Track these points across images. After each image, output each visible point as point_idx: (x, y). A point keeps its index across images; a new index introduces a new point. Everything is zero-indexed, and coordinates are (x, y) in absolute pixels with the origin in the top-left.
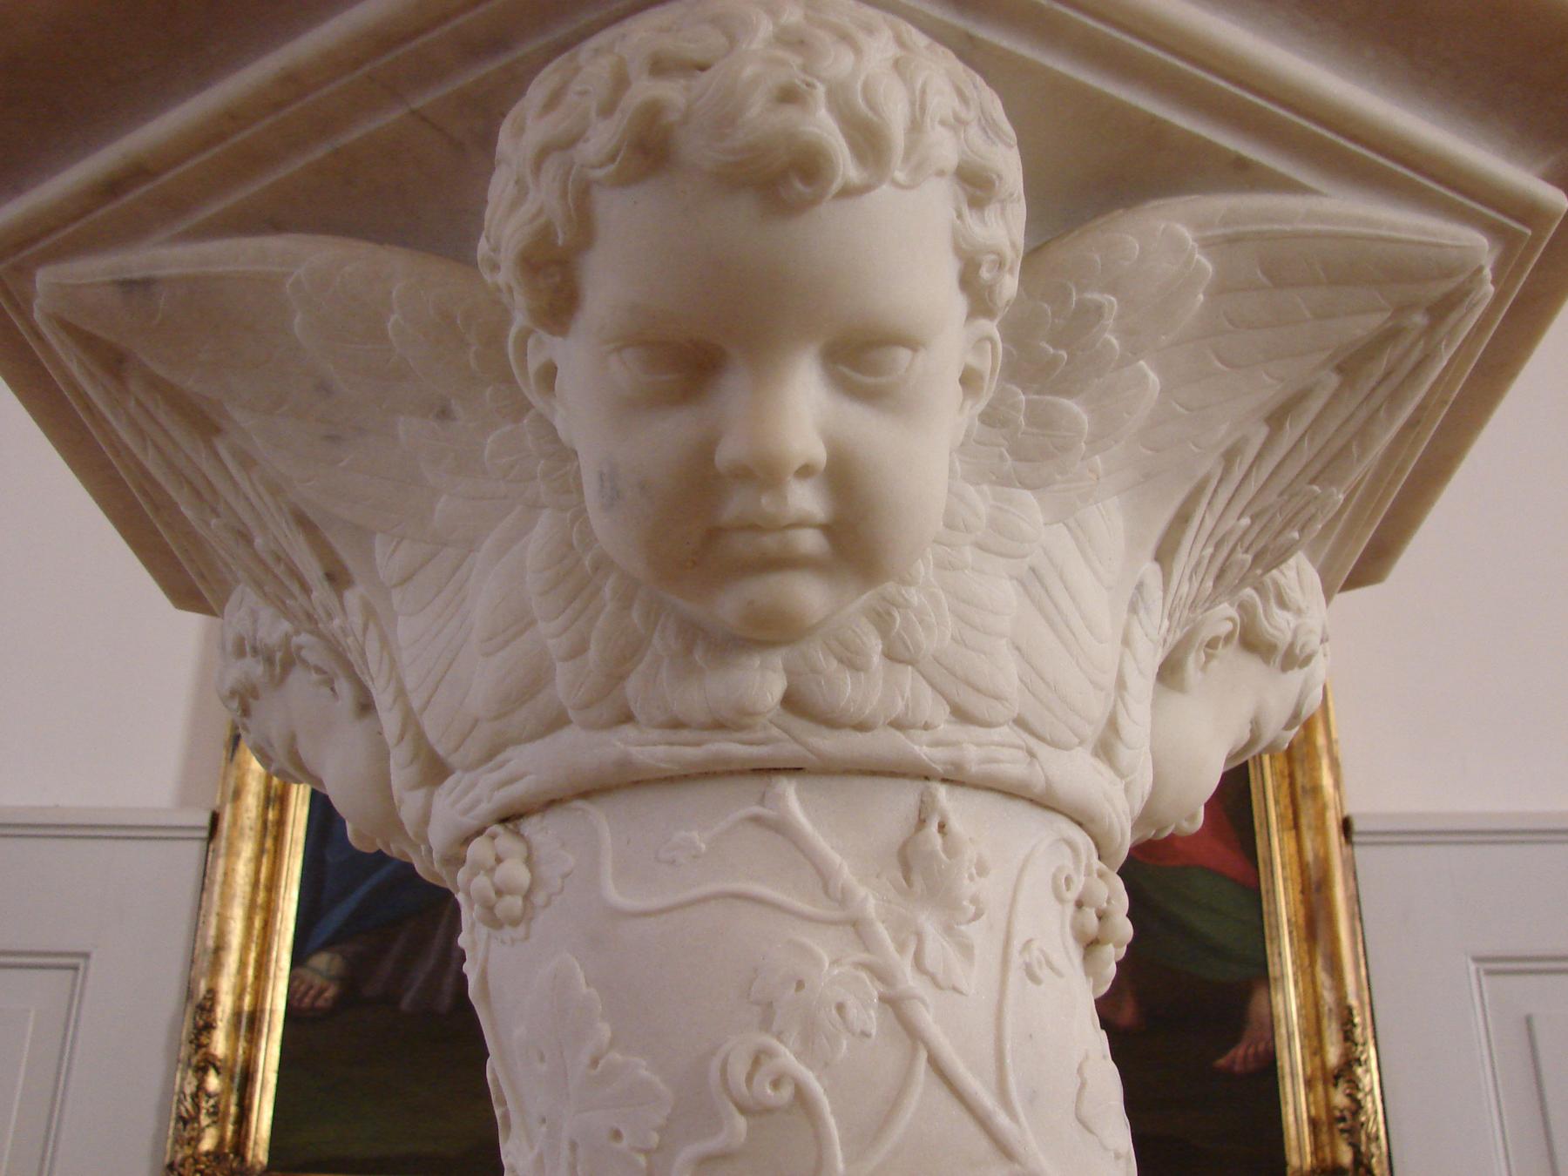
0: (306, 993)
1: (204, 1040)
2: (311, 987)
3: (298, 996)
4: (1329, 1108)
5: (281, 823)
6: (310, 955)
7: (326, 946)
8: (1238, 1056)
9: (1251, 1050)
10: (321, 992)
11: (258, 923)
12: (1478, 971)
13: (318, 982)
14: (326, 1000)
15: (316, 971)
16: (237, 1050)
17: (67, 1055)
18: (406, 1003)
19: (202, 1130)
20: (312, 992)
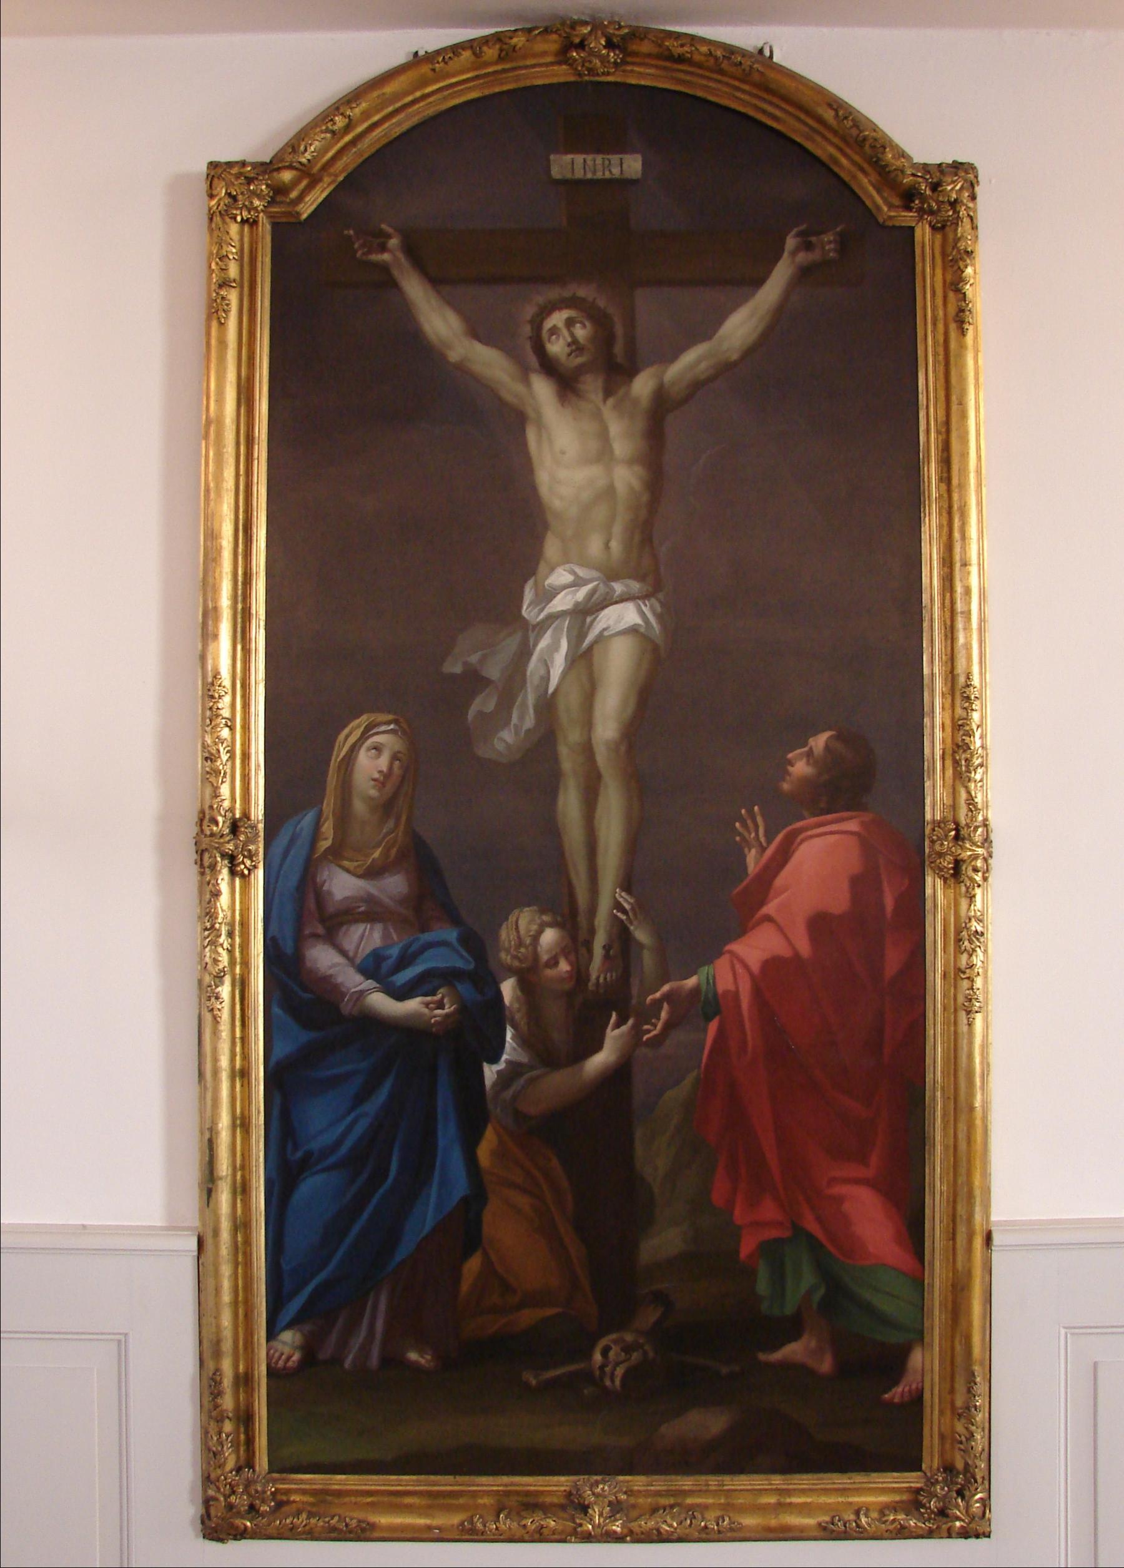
0: (280, 1358)
1: (219, 1401)
2: (282, 1354)
3: (274, 1361)
4: (953, 1431)
5: (247, 1242)
6: (278, 1334)
7: (289, 1326)
8: (897, 1393)
9: (907, 1389)
10: (289, 1358)
11: (241, 1311)
12: (1066, 1334)
13: (287, 1350)
14: (293, 1361)
15: (284, 1343)
16: (239, 1399)
17: (124, 1380)
18: (348, 1363)
19: (226, 1459)
20: (284, 1357)
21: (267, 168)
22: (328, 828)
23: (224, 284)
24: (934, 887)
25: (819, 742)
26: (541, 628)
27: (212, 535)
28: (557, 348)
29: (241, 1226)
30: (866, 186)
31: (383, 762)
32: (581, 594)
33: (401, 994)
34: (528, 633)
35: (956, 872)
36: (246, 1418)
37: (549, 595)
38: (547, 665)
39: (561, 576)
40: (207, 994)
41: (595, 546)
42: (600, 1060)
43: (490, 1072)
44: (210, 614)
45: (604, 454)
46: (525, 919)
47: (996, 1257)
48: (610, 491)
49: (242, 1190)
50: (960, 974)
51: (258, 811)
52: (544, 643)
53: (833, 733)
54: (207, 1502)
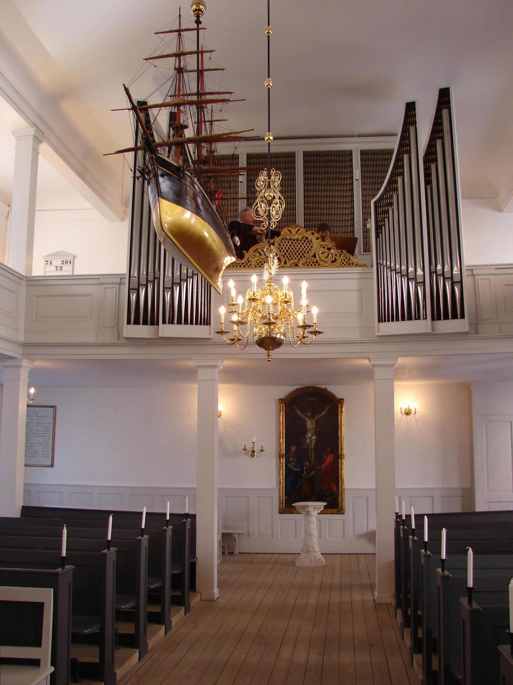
8: (337, 502)
21: (284, 399)
22: (290, 455)
23: (281, 410)
24: (340, 460)
25: (330, 448)
26: (307, 438)
27: (280, 431)
28: (309, 415)
29: (283, 487)
30: (335, 401)
31: (294, 449)
32: (310, 435)
33: (296, 468)
34: (306, 439)
35: (341, 459)
36: (283, 504)
37: (308, 436)
38: (308, 441)
39: (309, 434)
40: (280, 468)
41: (312, 432)
42: (312, 474)
43: (303, 475)
44: (280, 437)
45: (312, 424)
46: (306, 462)
47: (345, 491)
48: (313, 427)
49: (283, 484)
50: (341, 467)
51: (284, 453)
52: (307, 440)
53: (324, 564)
54: (280, 511)
